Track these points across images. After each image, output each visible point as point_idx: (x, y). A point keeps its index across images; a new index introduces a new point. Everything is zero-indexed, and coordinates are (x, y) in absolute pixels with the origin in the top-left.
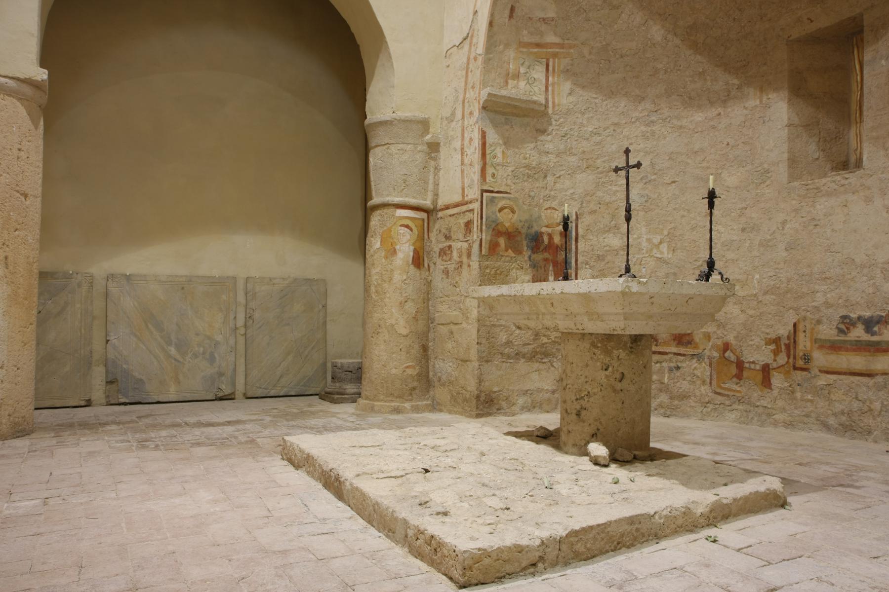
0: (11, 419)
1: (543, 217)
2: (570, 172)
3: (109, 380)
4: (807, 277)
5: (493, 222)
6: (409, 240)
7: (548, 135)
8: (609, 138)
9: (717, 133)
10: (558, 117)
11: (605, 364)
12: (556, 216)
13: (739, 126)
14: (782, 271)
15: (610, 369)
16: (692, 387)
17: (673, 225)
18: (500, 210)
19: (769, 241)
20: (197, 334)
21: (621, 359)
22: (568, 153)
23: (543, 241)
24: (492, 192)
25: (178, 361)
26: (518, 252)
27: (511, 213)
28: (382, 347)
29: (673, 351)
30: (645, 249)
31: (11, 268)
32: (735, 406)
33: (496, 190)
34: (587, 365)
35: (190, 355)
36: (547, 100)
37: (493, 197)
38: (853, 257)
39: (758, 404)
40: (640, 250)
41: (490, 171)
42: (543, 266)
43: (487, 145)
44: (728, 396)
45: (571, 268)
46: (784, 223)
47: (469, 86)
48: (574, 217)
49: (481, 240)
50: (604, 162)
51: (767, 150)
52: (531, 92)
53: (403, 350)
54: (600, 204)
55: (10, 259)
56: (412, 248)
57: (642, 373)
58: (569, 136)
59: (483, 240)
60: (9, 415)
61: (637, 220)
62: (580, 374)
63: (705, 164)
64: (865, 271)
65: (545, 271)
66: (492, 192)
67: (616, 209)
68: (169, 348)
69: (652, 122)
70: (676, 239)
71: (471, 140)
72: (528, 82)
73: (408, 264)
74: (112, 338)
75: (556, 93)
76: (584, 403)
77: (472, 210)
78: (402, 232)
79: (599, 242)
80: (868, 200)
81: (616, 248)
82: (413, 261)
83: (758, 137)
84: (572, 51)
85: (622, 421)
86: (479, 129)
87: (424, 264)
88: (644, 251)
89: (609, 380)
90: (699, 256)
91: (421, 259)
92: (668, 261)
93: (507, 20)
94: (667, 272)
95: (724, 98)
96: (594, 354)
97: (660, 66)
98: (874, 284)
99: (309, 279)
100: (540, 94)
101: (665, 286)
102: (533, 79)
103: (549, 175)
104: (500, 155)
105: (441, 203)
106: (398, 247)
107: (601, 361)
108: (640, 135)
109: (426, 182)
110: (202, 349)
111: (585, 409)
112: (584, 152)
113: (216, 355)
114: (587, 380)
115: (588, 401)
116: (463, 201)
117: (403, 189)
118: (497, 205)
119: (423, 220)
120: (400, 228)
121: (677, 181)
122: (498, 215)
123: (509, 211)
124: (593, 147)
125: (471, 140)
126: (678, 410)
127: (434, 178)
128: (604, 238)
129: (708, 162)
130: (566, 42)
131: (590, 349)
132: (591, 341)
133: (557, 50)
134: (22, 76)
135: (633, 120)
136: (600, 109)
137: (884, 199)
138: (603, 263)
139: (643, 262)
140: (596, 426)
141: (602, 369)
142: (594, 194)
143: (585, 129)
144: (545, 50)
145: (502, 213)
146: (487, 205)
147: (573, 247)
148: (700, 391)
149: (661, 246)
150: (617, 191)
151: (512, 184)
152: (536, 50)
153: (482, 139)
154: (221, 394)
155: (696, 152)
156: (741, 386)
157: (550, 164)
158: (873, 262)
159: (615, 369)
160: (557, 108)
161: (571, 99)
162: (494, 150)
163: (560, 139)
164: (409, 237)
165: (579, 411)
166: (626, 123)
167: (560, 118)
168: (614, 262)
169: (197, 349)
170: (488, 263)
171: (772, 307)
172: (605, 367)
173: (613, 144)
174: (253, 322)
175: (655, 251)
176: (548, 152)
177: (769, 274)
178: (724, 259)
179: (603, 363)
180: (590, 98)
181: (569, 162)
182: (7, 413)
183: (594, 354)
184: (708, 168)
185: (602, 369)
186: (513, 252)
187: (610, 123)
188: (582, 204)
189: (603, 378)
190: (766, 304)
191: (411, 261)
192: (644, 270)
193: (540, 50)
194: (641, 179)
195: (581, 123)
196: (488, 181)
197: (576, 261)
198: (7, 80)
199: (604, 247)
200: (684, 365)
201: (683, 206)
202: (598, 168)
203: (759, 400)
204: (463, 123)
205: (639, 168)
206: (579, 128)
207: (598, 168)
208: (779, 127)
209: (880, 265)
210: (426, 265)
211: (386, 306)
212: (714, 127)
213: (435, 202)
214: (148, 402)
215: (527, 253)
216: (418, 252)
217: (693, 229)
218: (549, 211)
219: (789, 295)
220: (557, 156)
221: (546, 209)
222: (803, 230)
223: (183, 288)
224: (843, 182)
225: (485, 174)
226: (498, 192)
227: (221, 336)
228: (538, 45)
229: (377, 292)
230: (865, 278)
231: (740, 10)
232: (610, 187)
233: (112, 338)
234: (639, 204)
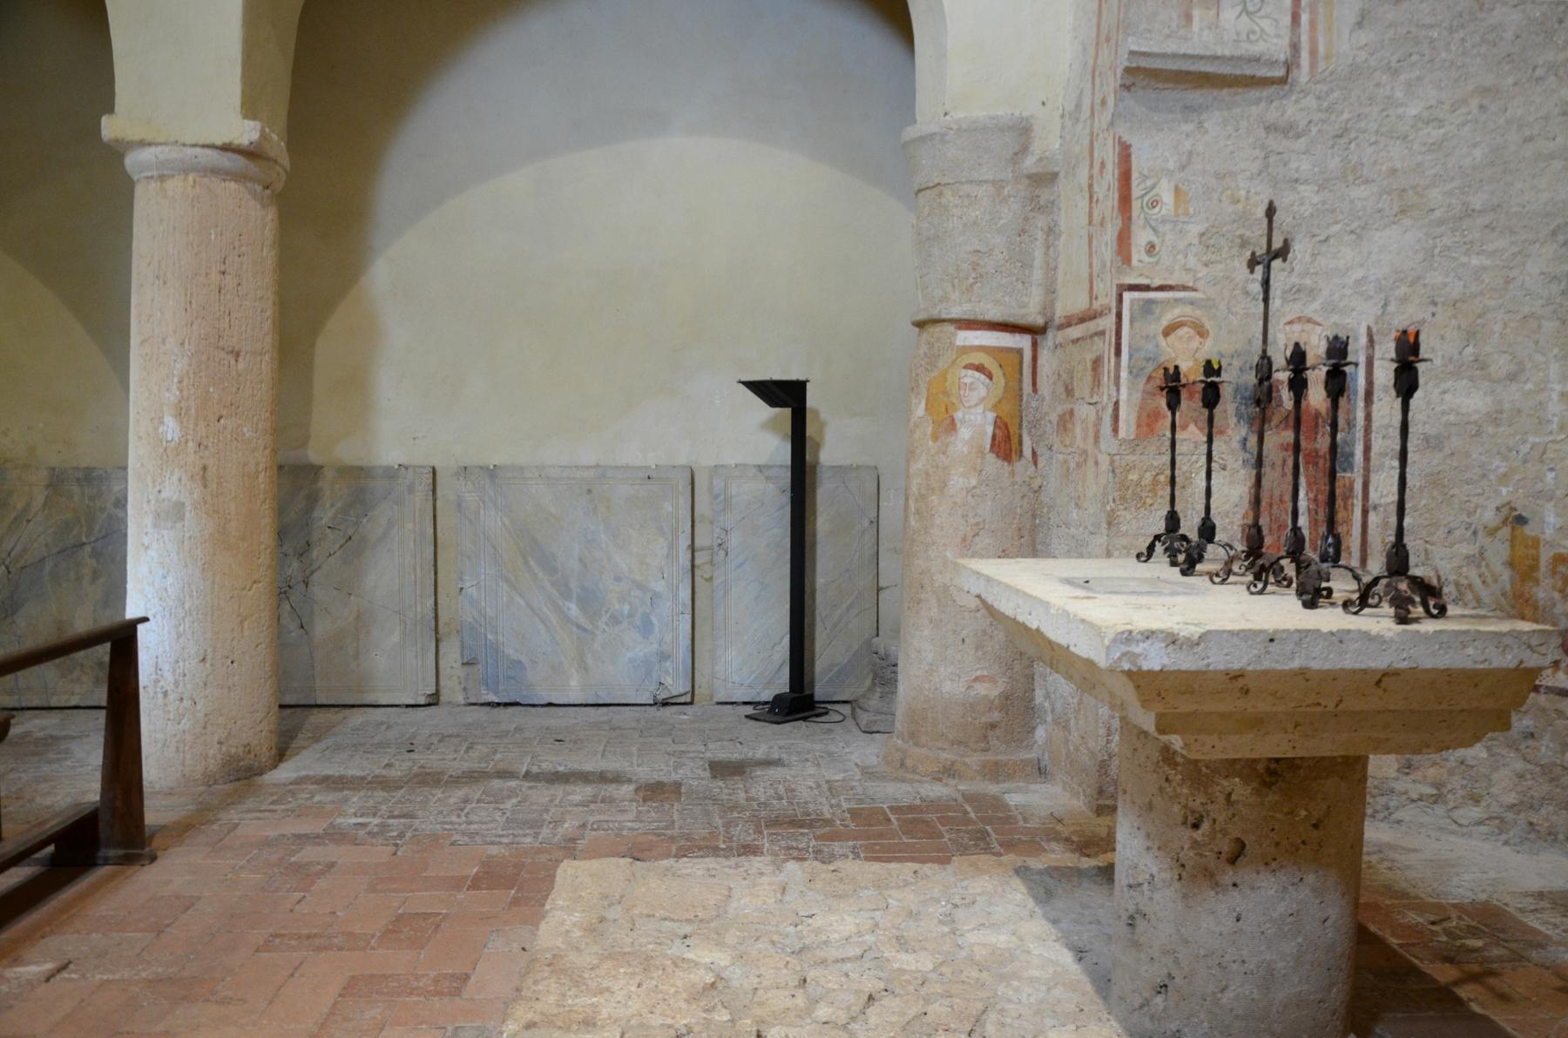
0: (224, 749)
2: (1355, 225)
3: (465, 661)
5: (1149, 359)
6: (984, 398)
7: (1298, 136)
8: (1466, 128)
10: (1325, 88)
11: (1193, 812)
15: (1206, 826)
18: (1167, 332)
20: (618, 579)
21: (1237, 802)
22: (1351, 178)
23: (1280, 404)
24: (1147, 288)
25: (585, 630)
27: (1198, 337)
28: (926, 633)
30: (1556, 419)
31: (213, 486)
33: (1157, 282)
35: (605, 618)
36: (1295, 47)
37: (1150, 302)
40: (1543, 422)
41: (1141, 237)
42: (1279, 462)
43: (1135, 176)
45: (1350, 467)
47: (1103, 38)
48: (1363, 340)
49: (1117, 404)
50: (1450, 194)
52: (1254, 32)
53: (967, 640)
54: (1435, 304)
55: (212, 471)
56: (991, 416)
57: (1304, 843)
58: (1353, 135)
59: (1121, 403)
60: (219, 743)
61: (1537, 343)
66: (1147, 288)
67: (1480, 316)
68: (567, 604)
71: (1103, 165)
72: (1245, 9)
73: (981, 453)
74: (468, 584)
75: (1320, 27)
77: (1102, 333)
78: (968, 380)
81: (1475, 417)
82: (993, 445)
85: (1235, 967)
86: (1114, 138)
87: (1021, 451)
88: (1555, 426)
89: (1201, 855)
91: (1015, 440)
96: (1167, 780)
99: (841, 467)
100: (1278, 36)
101: (1273, 647)
104: (1167, 197)
105: (1060, 312)
106: (959, 415)
107: (1183, 801)
108: (1557, 111)
109: (1027, 265)
110: (626, 608)
112: (1393, 171)
113: (654, 620)
116: (1089, 309)
117: (971, 286)
118: (1159, 318)
119: (1020, 352)
120: (964, 372)
122: (1163, 343)
123: (1192, 332)
124: (1420, 159)
125: (1103, 165)
127: (1046, 254)
128: (1444, 392)
134: (219, 142)
135: (1538, 73)
136: (1444, 55)
139: (1550, 455)
140: (1166, 966)
141: (1184, 823)
142: (1419, 278)
143: (1400, 111)
145: (1172, 337)
146: (1132, 322)
147: (1360, 415)
150: (1485, 268)
153: (1120, 162)
154: (662, 696)
157: (1303, 208)
159: (1218, 827)
160: (1322, 66)
161: (1364, 37)
162: (1153, 187)
163: (1331, 143)
164: (982, 392)
166: (1516, 84)
167: (1332, 91)
168: (1468, 455)
169: (617, 606)
170: (1134, 458)
172: (1191, 819)
173: (1475, 145)
174: (727, 554)
176: (1296, 181)
179: (1186, 807)
180: (1413, 29)
181: (1352, 201)
182: (216, 738)
185: (1184, 823)
187: (1470, 88)
188: (1386, 305)
189: (1186, 847)
191: (988, 446)
192: (1550, 476)
194: (1554, 233)
195: (1389, 98)
196: (1134, 262)
197: (1367, 449)
198: (198, 150)
199: (1443, 413)
202: (1433, 210)
204: (1092, 125)
206: (1383, 110)
207: (1433, 210)
210: (1027, 452)
211: (934, 544)
213: (1048, 306)
214: (531, 702)
216: (1006, 425)
220: (1322, 188)
221: (1290, 323)
223: (589, 491)
225: (1129, 245)
226: (1161, 288)
227: (663, 582)
229: (918, 512)
232: (1464, 259)
233: (468, 584)
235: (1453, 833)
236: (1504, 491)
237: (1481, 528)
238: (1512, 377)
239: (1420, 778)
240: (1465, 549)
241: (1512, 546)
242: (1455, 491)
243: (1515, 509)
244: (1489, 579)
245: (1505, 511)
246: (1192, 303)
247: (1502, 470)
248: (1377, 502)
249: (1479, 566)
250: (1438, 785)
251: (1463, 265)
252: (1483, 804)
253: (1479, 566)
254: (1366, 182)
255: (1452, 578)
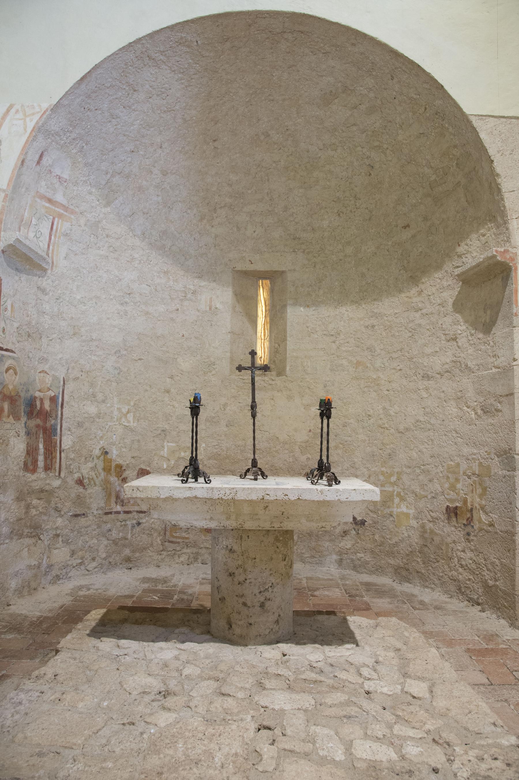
1: (37, 381)
4: (242, 448)
9: (174, 325)
12: (47, 380)
13: (192, 323)
14: (222, 442)
16: (150, 539)
17: (138, 397)
19: (214, 418)
22: (60, 317)
23: (36, 406)
26: (17, 418)
29: (136, 510)
30: (116, 417)
32: (185, 550)
34: (272, 559)
37: (3, 356)
38: (277, 436)
39: (202, 546)
40: (112, 418)
44: (179, 543)
46: (225, 405)
51: (213, 347)
54: (82, 372)
58: (61, 300)
61: (110, 390)
62: (264, 568)
63: (164, 349)
64: (287, 446)
65: (36, 438)
67: (94, 378)
69: (126, 303)
70: (140, 409)
76: (267, 594)
79: (79, 409)
80: (290, 398)
81: (93, 415)
83: (207, 336)
84: (72, 217)
88: (115, 420)
90: (158, 426)
92: (134, 429)
93: (35, 164)
94: (132, 439)
95: (181, 298)
97: (136, 256)
98: (294, 455)
102: (40, 233)
103: (43, 336)
108: (116, 312)
111: (269, 600)
114: (272, 572)
115: (272, 592)
121: (142, 359)
126: (139, 561)
128: (84, 405)
129: (167, 347)
130: (72, 207)
131: (274, 543)
132: (275, 536)
133: (62, 212)
135: (111, 297)
137: (302, 400)
138: (82, 429)
144: (53, 208)
148: (156, 541)
149: (128, 415)
151: (16, 343)
152: (47, 205)
155: (158, 337)
156: (189, 533)
158: (293, 441)
163: (55, 301)
165: (263, 603)
171: (214, 470)
173: (94, 316)
175: (123, 419)
177: (213, 444)
178: (177, 429)
183: (277, 547)
184: (168, 352)
186: (13, 418)
190: (209, 467)
192: (115, 436)
193: (50, 206)
200: (144, 521)
201: (146, 381)
203: (203, 543)
205: (240, 365)
208: (224, 332)
209: (299, 443)
212: (172, 319)
215: (24, 419)
217: (154, 402)
218: (42, 374)
219: (227, 461)
221: (40, 372)
222: (240, 412)
224: (271, 382)
228: (50, 201)
230: (286, 451)
231: (200, 234)
232: (90, 356)
234: (113, 376)
235: (87, 575)
236: (101, 442)
237: (95, 456)
238: (103, 401)
239: (77, 557)
240: (90, 465)
241: (104, 463)
242: (87, 443)
243: (105, 449)
244: (98, 475)
245: (102, 450)
246: (14, 358)
247: (101, 435)
248: (64, 448)
249: (95, 471)
250: (82, 558)
251: (89, 358)
252: (96, 560)
253: (95, 471)
254: (64, 320)
255: (87, 476)
